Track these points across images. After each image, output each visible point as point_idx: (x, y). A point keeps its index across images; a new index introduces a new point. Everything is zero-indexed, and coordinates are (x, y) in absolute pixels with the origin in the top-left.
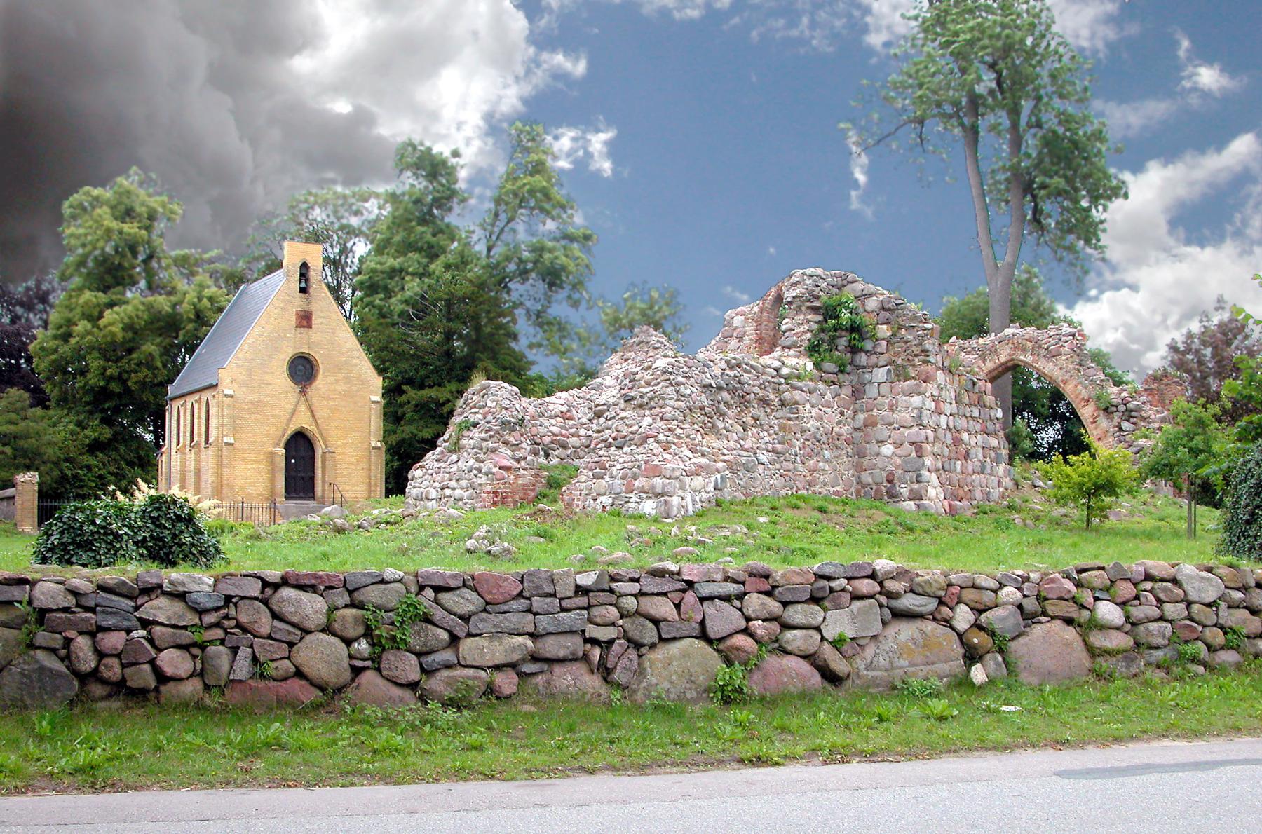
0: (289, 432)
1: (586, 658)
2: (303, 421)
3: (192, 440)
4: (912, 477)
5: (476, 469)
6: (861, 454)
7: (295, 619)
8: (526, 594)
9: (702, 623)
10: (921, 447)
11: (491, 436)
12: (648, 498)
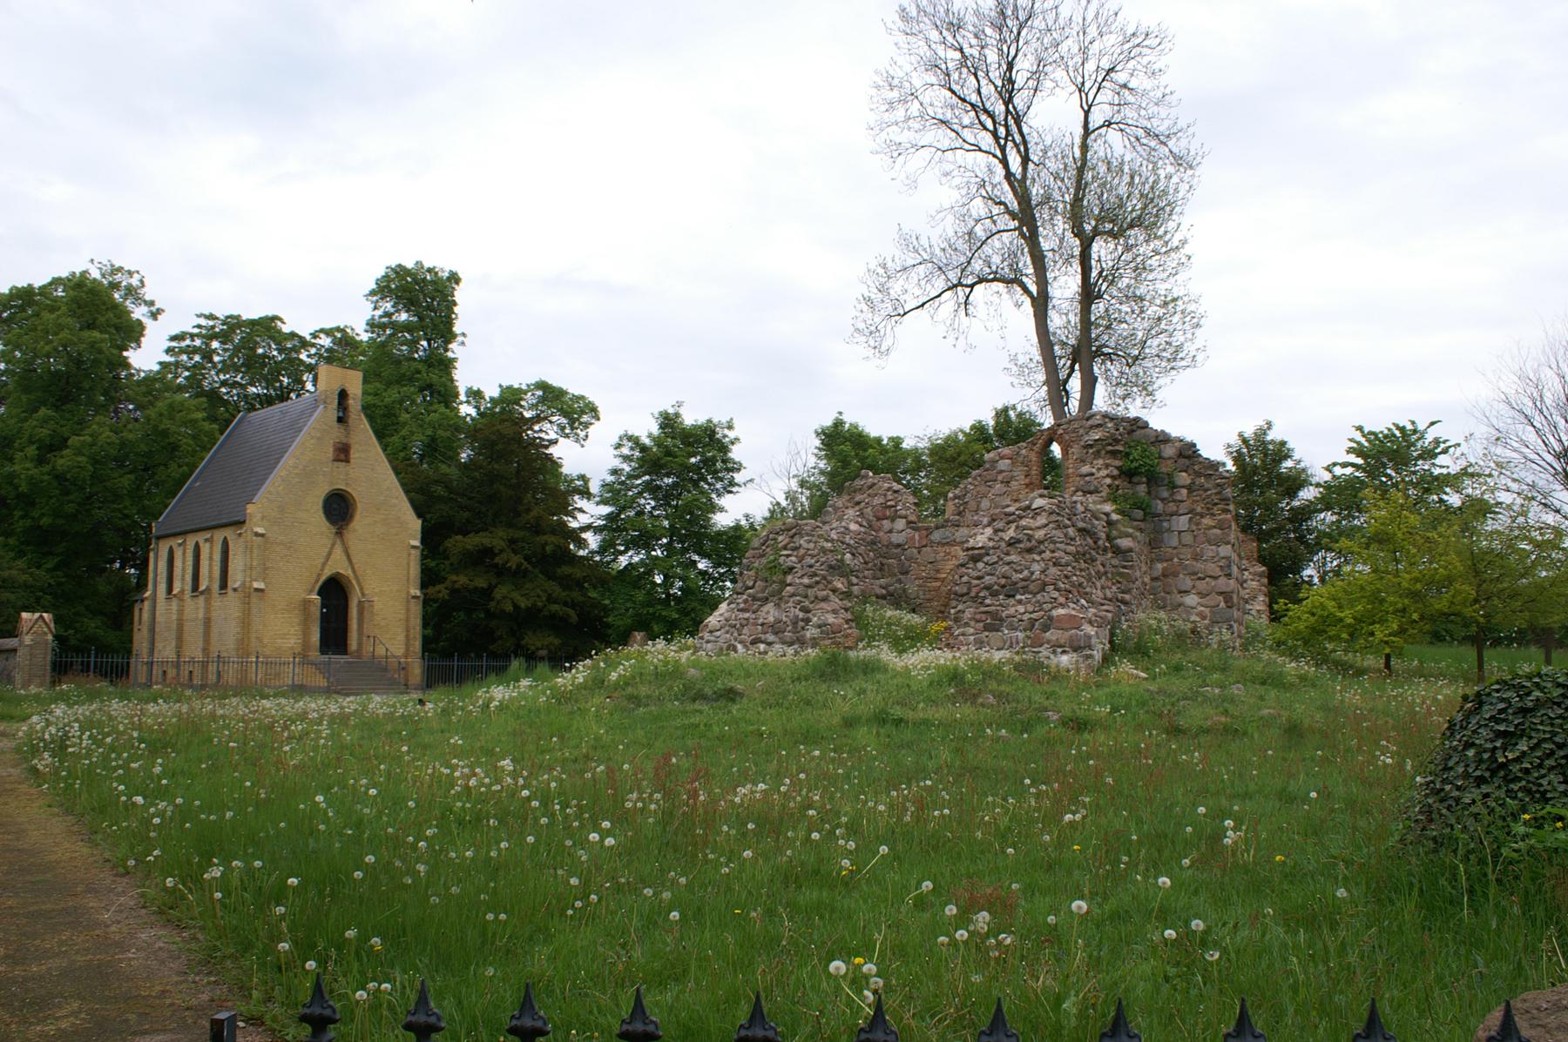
0: (323, 578)
2: (337, 565)
5: (802, 620)
11: (817, 583)
12: (1064, 652)
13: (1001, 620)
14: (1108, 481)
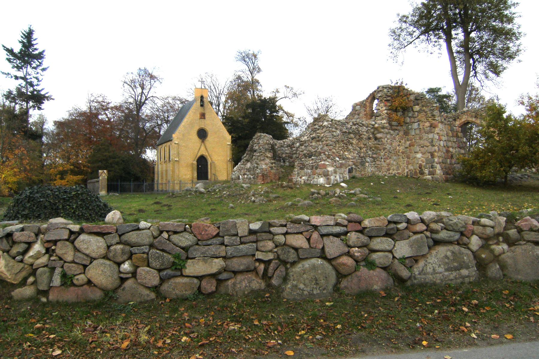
0: (198, 156)
1: (255, 270)
2: (203, 152)
3: (165, 160)
4: (429, 166)
6: (408, 157)
7: (87, 252)
8: (221, 234)
9: (323, 248)
10: (433, 154)
11: (262, 155)
12: (322, 177)
13: (305, 166)
14: (386, 111)
